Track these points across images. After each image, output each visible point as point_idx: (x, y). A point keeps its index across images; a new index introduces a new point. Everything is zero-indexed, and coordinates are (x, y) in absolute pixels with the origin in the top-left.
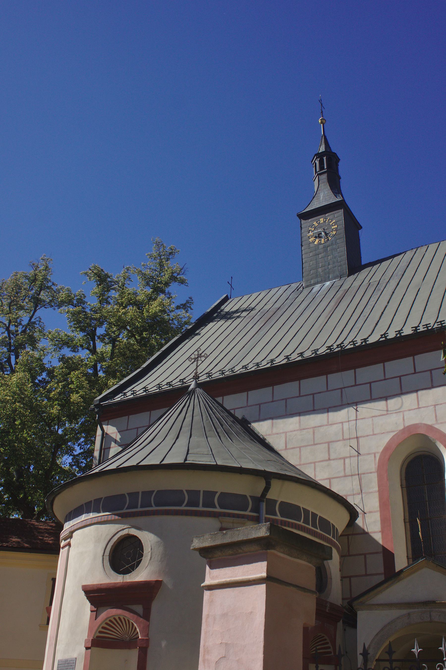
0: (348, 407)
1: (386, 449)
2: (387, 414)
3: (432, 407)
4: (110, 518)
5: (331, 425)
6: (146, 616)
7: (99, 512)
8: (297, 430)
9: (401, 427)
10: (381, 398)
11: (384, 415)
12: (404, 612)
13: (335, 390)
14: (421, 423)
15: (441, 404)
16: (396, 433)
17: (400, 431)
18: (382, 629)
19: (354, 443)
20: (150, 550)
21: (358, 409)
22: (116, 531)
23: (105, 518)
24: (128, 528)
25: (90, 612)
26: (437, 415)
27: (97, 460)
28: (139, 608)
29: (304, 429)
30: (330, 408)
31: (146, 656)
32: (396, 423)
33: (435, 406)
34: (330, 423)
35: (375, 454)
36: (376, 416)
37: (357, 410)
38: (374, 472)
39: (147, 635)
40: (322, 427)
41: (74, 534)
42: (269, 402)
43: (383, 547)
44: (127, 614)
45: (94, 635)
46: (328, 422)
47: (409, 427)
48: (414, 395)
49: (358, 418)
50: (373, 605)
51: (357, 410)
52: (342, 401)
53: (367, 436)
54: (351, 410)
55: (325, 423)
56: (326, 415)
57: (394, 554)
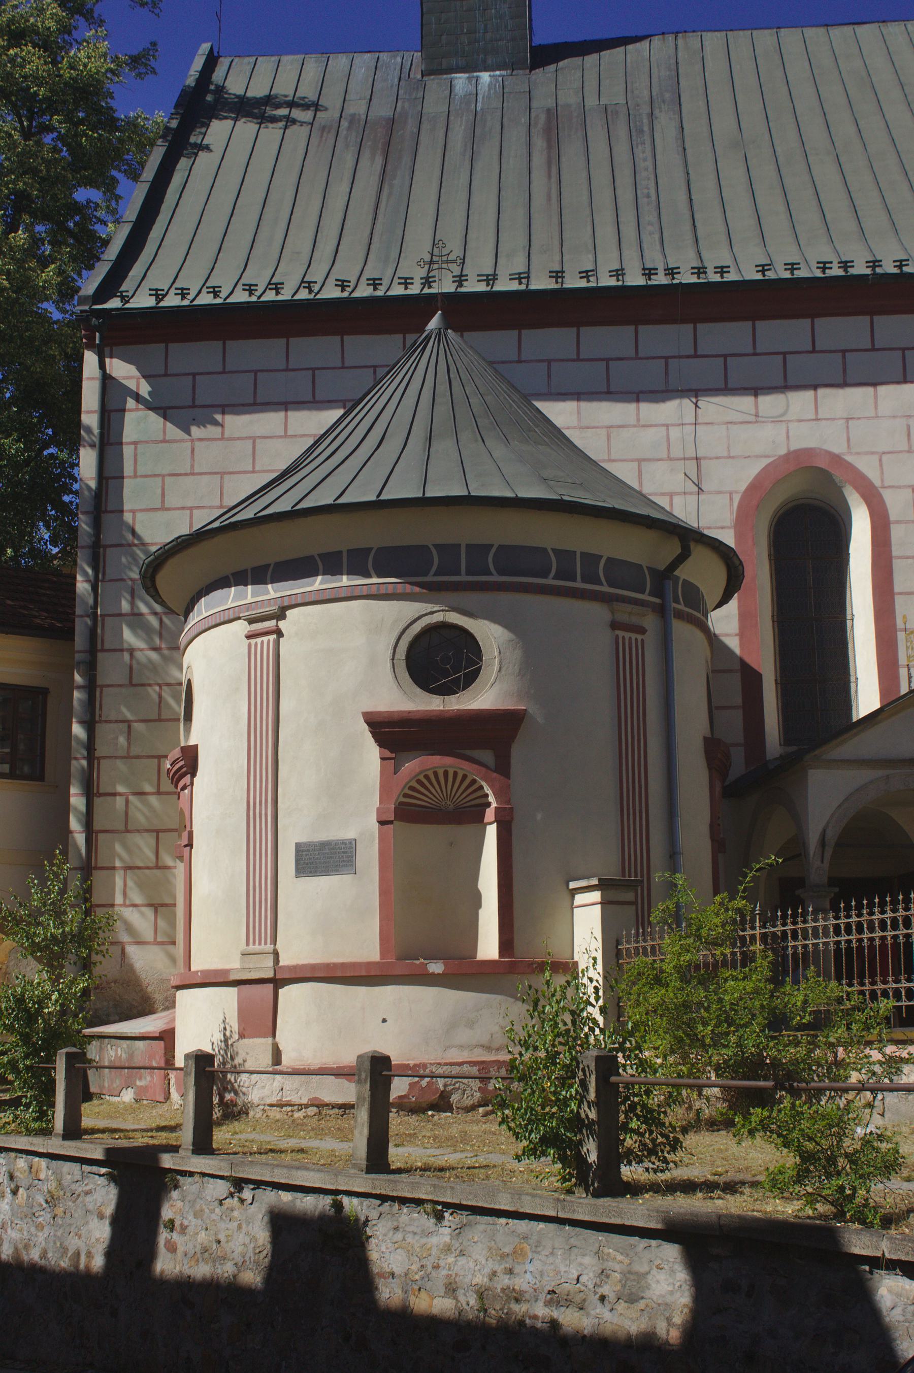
0: (681, 397)
1: (754, 487)
2: (757, 422)
3: (843, 421)
4: (400, 589)
5: (643, 426)
6: (503, 768)
7: (369, 576)
8: (574, 428)
9: (783, 451)
10: (746, 389)
11: (750, 422)
12: (879, 773)
13: (654, 358)
14: (820, 449)
15: (859, 418)
16: (771, 460)
17: (780, 457)
18: (847, 799)
19: (691, 467)
20: (496, 653)
21: (699, 404)
22: (417, 616)
23: (390, 589)
24: (443, 611)
25: (379, 760)
26: (851, 438)
27: (93, 434)
28: (487, 756)
29: (588, 428)
30: (642, 392)
31: (511, 835)
32: (774, 442)
33: (848, 419)
34: (642, 423)
35: (731, 494)
36: (735, 423)
37: (697, 406)
38: (728, 528)
39: (509, 802)
40: (626, 429)
41: (288, 613)
42: (511, 362)
43: (743, 664)
44: (465, 766)
45: (397, 800)
46: (638, 420)
47: (795, 451)
48: (809, 394)
49: (699, 421)
50: (834, 761)
51: (697, 406)
52: (667, 382)
53: (717, 458)
54: (687, 404)
55: (633, 421)
56: (632, 406)
57: (761, 675)
